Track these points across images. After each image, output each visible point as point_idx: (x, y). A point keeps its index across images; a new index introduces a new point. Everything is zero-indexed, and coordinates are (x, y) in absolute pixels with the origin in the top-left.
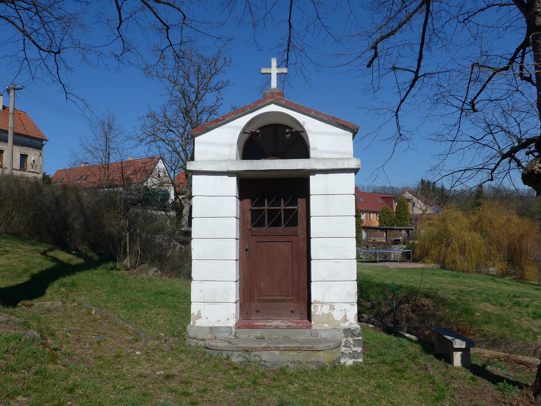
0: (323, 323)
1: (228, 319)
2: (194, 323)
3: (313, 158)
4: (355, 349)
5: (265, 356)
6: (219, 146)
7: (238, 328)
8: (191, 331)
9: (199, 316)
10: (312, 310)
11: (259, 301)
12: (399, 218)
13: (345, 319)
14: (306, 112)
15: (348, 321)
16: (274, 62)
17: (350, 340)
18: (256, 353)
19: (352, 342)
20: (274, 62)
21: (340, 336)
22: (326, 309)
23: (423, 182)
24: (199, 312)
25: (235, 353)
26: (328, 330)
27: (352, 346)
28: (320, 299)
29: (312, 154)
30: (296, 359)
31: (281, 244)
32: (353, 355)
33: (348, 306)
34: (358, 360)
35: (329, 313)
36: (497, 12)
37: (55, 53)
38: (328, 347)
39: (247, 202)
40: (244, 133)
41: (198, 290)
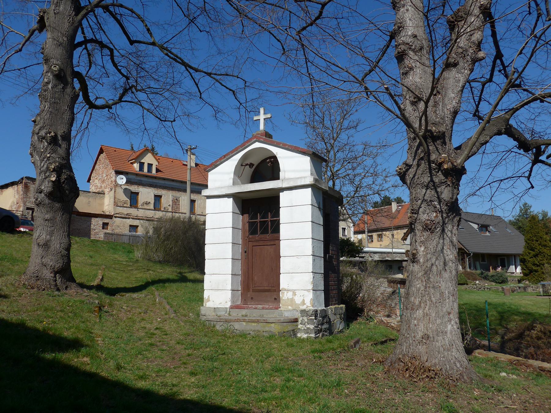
0: (288, 306)
2: (206, 305)
4: (308, 326)
5: (237, 326)
6: (223, 177)
7: (231, 308)
8: (203, 310)
9: (208, 300)
11: (254, 291)
13: (303, 303)
14: (277, 145)
16: (262, 111)
17: (305, 319)
18: (231, 323)
19: (306, 320)
20: (262, 111)
21: (297, 315)
22: (290, 295)
24: (209, 297)
25: (219, 323)
26: (290, 310)
27: (306, 324)
28: (286, 288)
30: (257, 328)
32: (307, 331)
33: (306, 293)
34: (310, 335)
35: (292, 298)
37: (172, 122)
38: (279, 320)
39: (246, 216)
40: (242, 165)
41: (208, 280)
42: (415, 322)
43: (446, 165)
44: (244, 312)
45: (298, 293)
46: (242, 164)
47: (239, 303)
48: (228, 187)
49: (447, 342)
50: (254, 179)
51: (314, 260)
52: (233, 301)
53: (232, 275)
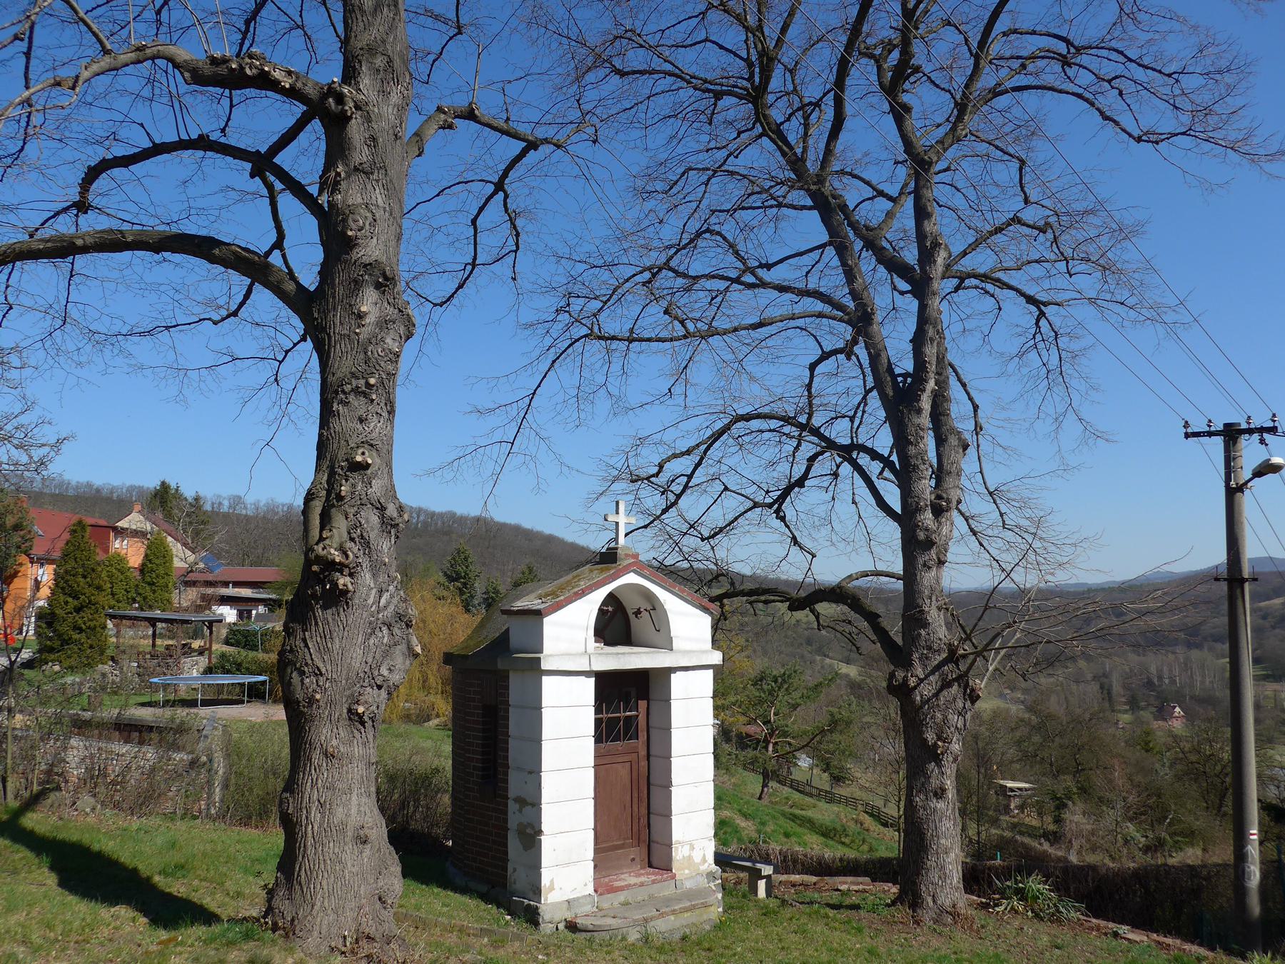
3: (680, 652)
9: (552, 888)
12: (151, 584)
13: (704, 860)
23: (163, 483)
24: (552, 881)
29: (675, 646)
31: (619, 766)
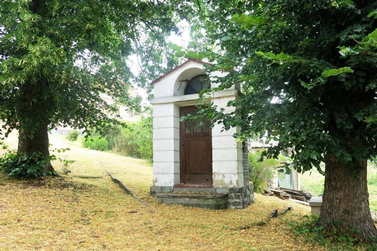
1: (170, 183)
4: (236, 200)
10: (213, 177)
13: (231, 183)
15: (232, 184)
19: (234, 196)
22: (220, 178)
27: (234, 198)
28: (217, 172)
30: (198, 203)
33: (233, 176)
36: (73, 162)
42: (338, 201)
43: (281, 63)
44: (185, 190)
45: (226, 176)
46: (180, 80)
47: (179, 182)
48: (170, 97)
49: (362, 216)
50: (188, 91)
51: (238, 151)
52: (175, 181)
53: (174, 162)
